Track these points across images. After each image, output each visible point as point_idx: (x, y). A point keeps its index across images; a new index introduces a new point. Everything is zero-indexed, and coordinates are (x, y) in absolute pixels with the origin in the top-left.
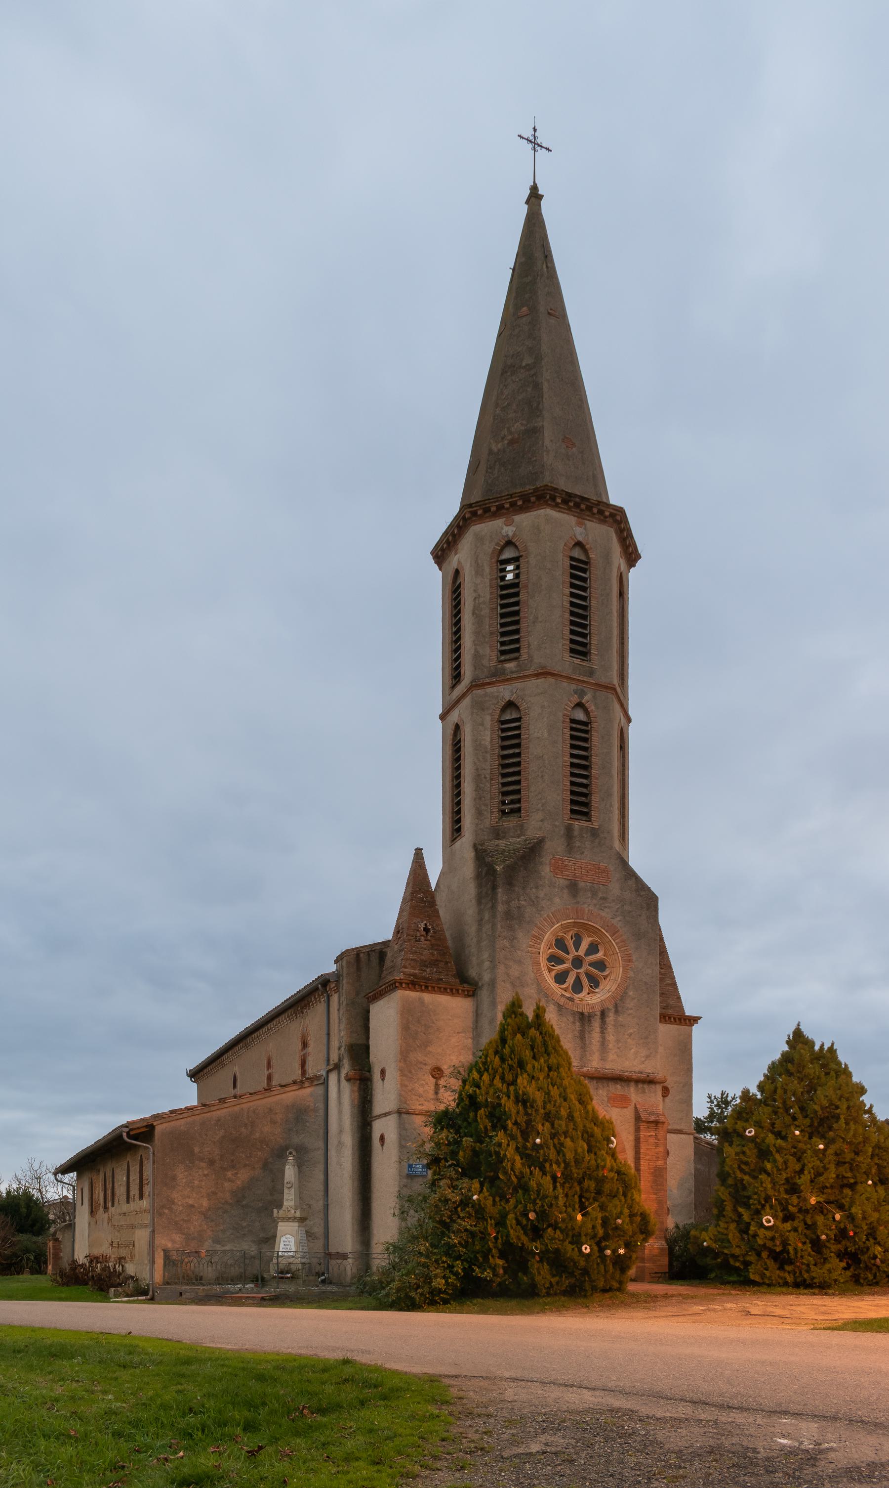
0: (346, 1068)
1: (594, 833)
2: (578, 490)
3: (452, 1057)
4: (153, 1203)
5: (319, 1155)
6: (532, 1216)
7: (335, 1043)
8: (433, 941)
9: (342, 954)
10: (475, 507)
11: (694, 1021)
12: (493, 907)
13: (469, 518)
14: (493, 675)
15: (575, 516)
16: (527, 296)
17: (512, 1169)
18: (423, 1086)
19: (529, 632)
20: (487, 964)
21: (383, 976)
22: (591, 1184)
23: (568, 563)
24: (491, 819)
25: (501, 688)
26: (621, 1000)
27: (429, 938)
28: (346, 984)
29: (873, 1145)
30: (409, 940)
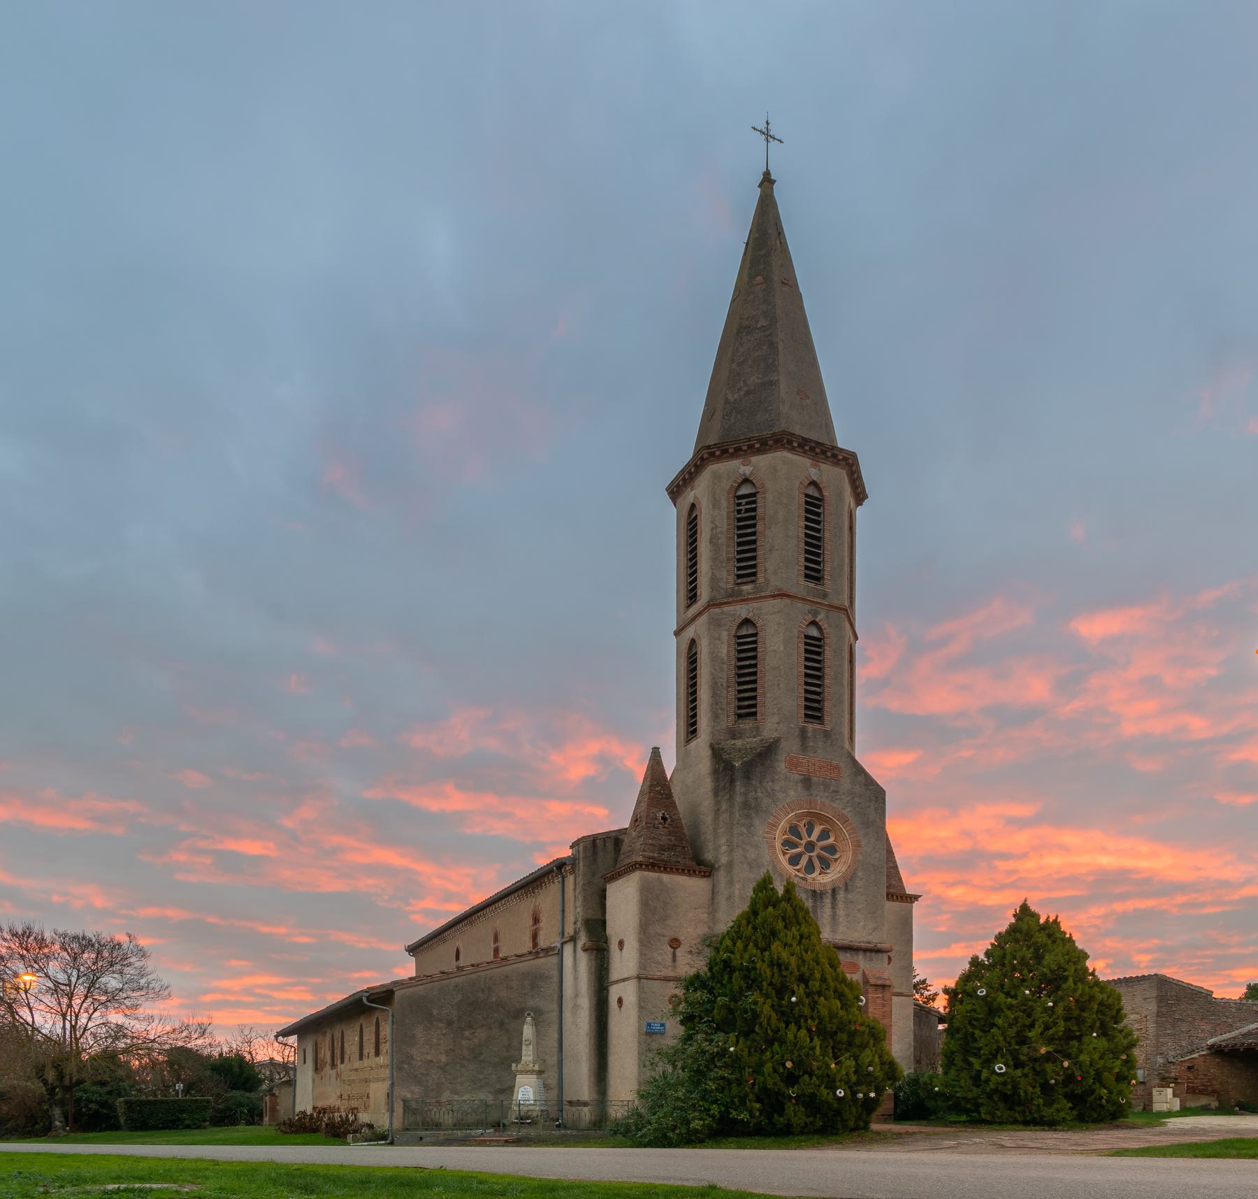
0: (583, 939)
1: (827, 735)
2: (813, 435)
3: (689, 930)
4: (392, 1061)
5: (554, 1016)
6: (789, 1065)
7: (570, 918)
8: (671, 829)
9: (579, 840)
10: (713, 448)
11: (915, 898)
12: (731, 798)
13: (707, 459)
14: (730, 596)
15: (810, 459)
16: (761, 267)
17: (768, 1024)
18: (661, 954)
19: (765, 559)
20: (724, 848)
21: (620, 859)
22: (843, 1037)
23: (803, 499)
24: (728, 721)
25: (738, 607)
26: (851, 880)
27: (667, 826)
28: (581, 865)
29: (1098, 1003)
30: (648, 828)
